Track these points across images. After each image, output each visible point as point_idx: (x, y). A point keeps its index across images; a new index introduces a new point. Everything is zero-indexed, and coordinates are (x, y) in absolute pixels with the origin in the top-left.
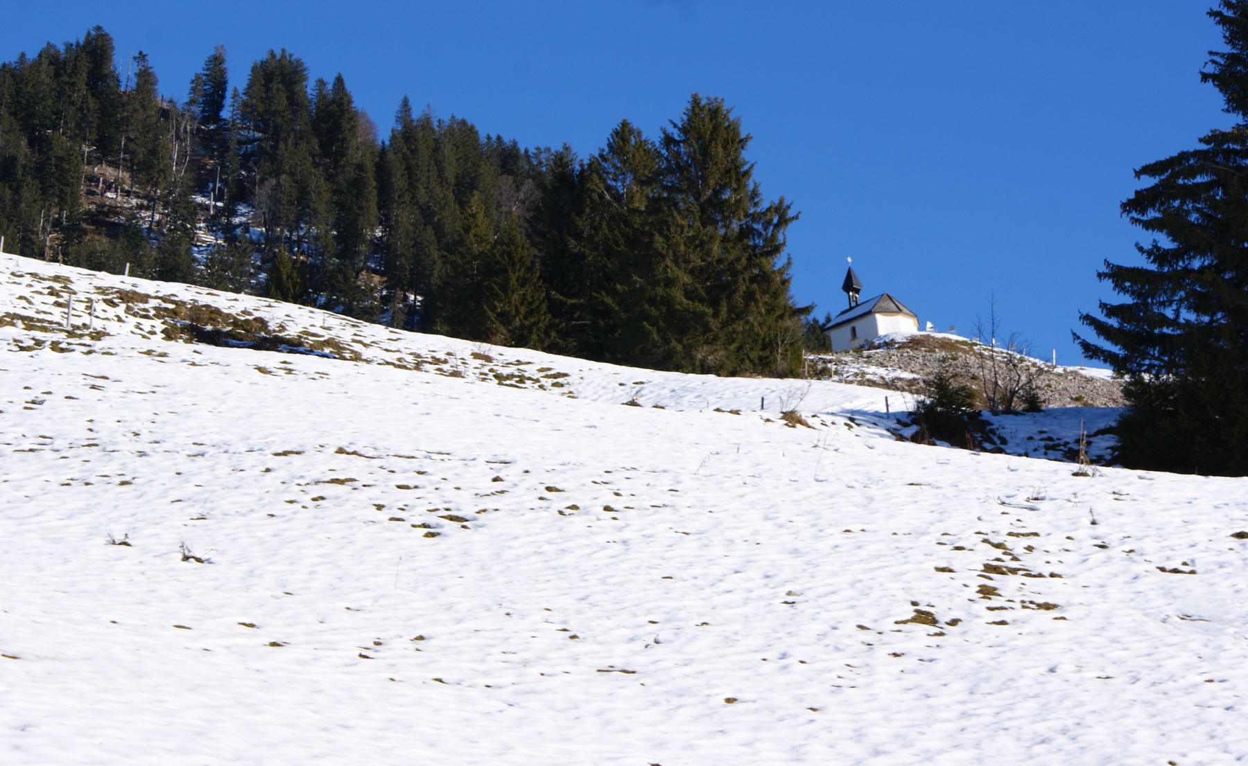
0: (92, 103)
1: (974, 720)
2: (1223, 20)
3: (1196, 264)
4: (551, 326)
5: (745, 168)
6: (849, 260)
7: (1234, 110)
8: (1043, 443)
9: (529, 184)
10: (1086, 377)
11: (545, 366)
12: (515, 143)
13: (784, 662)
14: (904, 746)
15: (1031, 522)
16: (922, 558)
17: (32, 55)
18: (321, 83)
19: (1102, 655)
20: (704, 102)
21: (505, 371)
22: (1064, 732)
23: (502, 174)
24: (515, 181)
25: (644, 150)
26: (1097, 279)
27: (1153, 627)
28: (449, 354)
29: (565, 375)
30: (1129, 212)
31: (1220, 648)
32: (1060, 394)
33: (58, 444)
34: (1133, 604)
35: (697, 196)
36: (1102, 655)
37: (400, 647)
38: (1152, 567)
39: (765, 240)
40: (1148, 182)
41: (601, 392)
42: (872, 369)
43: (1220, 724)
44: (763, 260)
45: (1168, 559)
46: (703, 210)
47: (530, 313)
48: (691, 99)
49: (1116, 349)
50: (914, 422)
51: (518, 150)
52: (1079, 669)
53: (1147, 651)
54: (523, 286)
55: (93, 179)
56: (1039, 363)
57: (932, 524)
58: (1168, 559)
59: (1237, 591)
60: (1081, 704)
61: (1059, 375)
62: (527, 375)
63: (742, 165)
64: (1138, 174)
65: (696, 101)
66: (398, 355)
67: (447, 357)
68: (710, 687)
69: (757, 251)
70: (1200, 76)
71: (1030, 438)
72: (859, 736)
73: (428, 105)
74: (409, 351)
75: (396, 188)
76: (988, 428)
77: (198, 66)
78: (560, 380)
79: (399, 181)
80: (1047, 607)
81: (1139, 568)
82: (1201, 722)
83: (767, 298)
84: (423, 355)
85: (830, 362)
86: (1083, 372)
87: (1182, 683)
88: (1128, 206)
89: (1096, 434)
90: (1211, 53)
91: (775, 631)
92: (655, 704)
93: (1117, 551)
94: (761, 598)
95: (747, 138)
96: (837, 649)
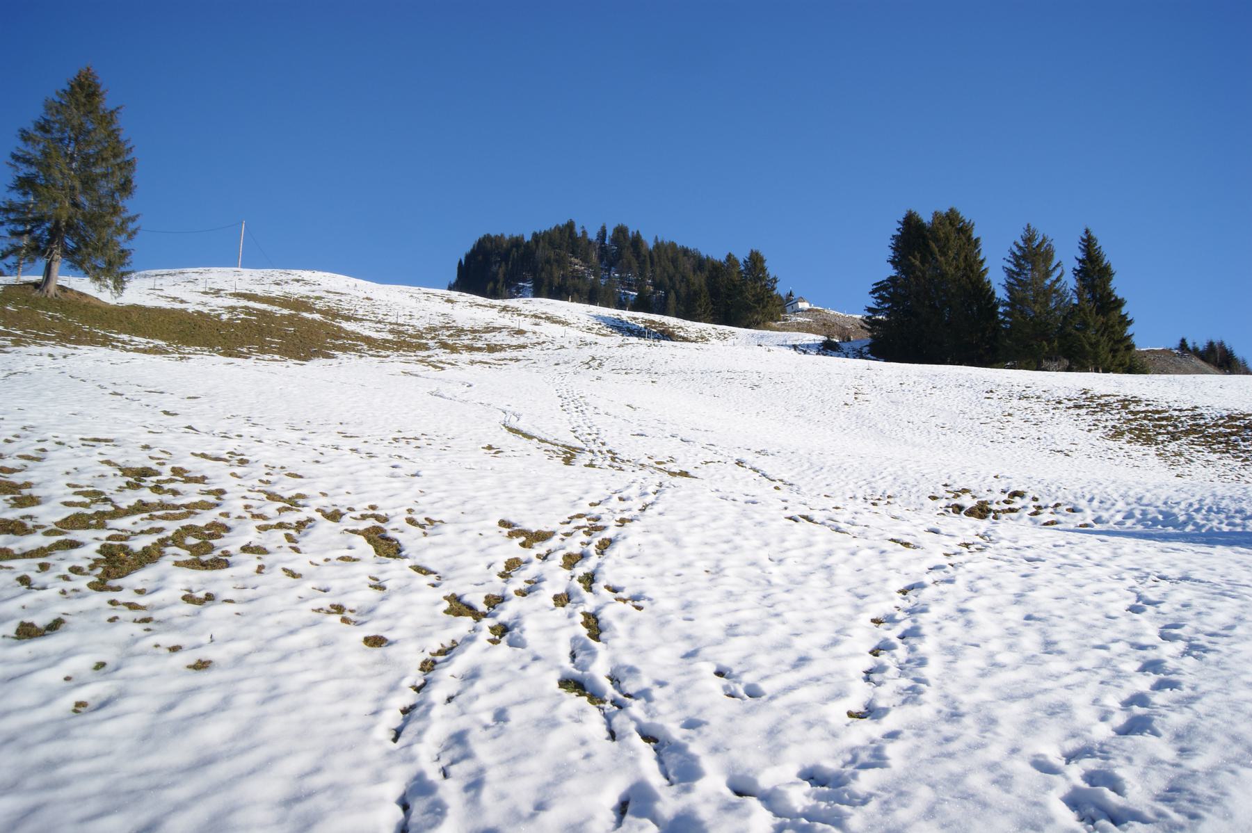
0: (570, 241)
3: (887, 306)
9: (692, 259)
17: (553, 228)
18: (633, 233)
27: (886, 404)
37: (762, 413)
40: (875, 287)
49: (869, 327)
55: (571, 263)
77: (599, 229)
79: (656, 260)
88: (870, 293)
93: (878, 388)
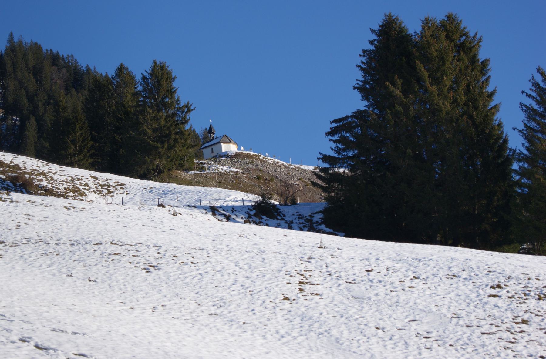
1: (304, 328)
2: (362, 69)
3: (351, 154)
4: (92, 146)
5: (174, 90)
6: (211, 121)
7: (365, 100)
8: (297, 217)
9: (64, 71)
10: (303, 170)
11: (117, 181)
12: (58, 52)
13: (254, 312)
14: (289, 335)
15: (310, 267)
16: (282, 279)
19: (333, 310)
20: (158, 63)
21: (103, 183)
22: (326, 331)
23: (53, 65)
24: (58, 69)
25: (129, 76)
26: (317, 160)
27: (345, 301)
28: (82, 176)
29: (124, 184)
30: (328, 136)
31: (363, 307)
32: (293, 177)
33: (33, 241)
34: (339, 293)
35: (155, 100)
36: (333, 310)
38: (344, 282)
39: (182, 118)
40: (334, 125)
41: (137, 192)
42: (221, 167)
43: (363, 329)
44: (181, 126)
45: (348, 279)
46: (157, 106)
47: (84, 141)
48: (153, 62)
49: (323, 184)
50: (254, 209)
51: (59, 56)
52: (328, 314)
53: (344, 308)
54: (81, 130)
56: (285, 163)
57: (282, 267)
58: (348, 279)
59: (367, 289)
60: (329, 324)
61: (293, 169)
62: (111, 184)
63: (173, 89)
64: (331, 123)
65: (155, 63)
66: (65, 177)
67: (82, 178)
68: (238, 319)
69: (179, 122)
70: (353, 88)
71: (293, 215)
72: (277, 332)
73: (21, 36)
74: (68, 176)
75: (8, 71)
76: (279, 211)
78: (123, 187)
80: (317, 294)
81: (340, 282)
82: (359, 329)
83: (182, 141)
84: (73, 177)
85: (205, 164)
86: (302, 167)
87: (354, 318)
88: (328, 134)
89: (316, 213)
90: (357, 80)
91: (249, 303)
92: (226, 324)
94: (243, 293)
95: (175, 78)
96: (266, 308)
